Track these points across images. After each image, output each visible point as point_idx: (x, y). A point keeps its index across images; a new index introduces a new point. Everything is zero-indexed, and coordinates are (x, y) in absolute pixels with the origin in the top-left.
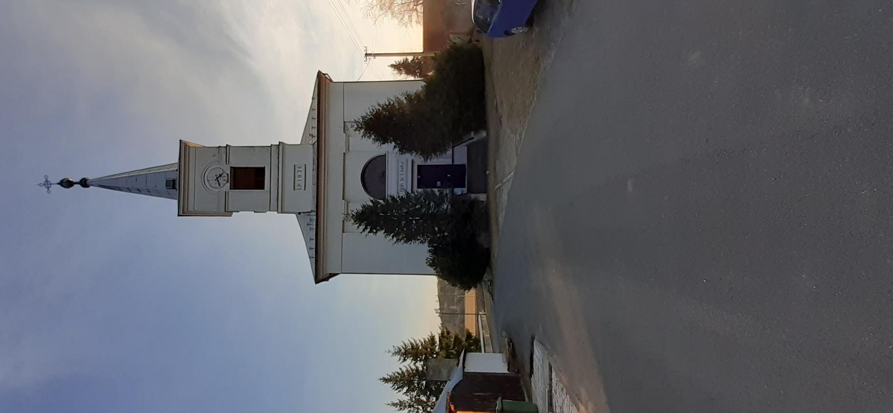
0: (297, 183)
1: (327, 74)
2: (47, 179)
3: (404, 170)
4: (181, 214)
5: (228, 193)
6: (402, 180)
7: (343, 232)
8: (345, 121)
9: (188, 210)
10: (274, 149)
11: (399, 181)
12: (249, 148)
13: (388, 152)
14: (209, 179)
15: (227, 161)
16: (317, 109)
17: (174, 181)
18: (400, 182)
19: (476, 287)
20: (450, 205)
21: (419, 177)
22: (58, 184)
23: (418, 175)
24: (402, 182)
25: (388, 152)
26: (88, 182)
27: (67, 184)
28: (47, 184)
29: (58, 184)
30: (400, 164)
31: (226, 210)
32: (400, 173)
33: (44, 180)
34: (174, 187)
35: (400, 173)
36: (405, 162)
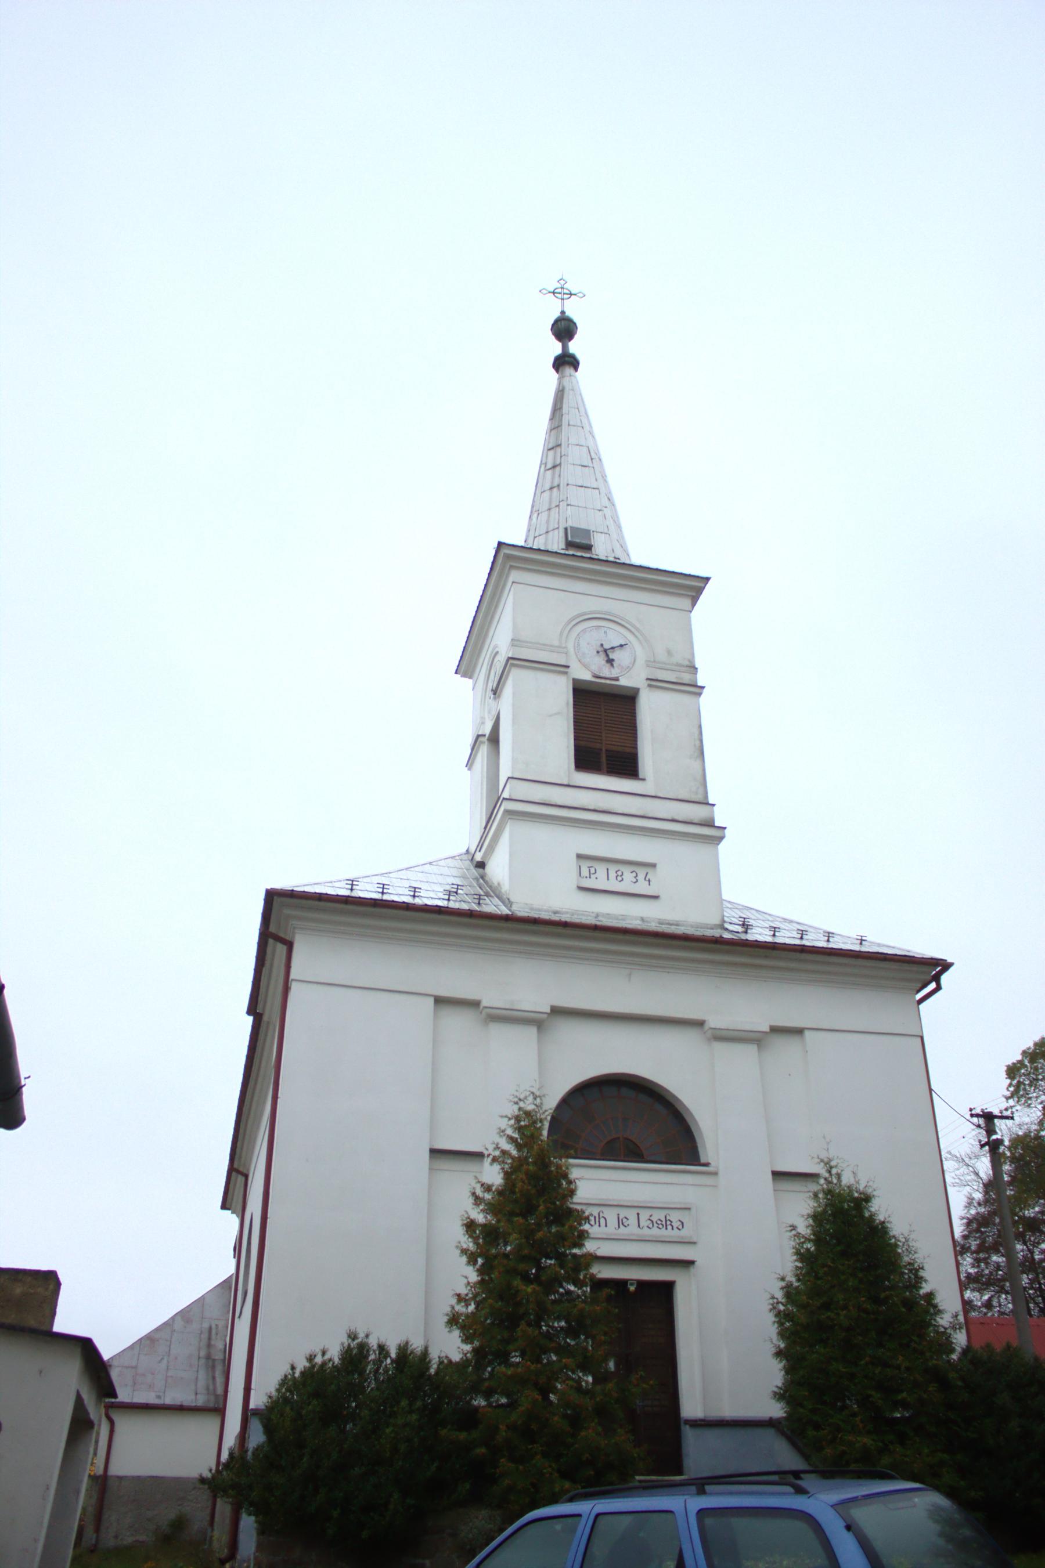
0: (601, 869)
1: (938, 988)
2: (575, 295)
3: (655, 1231)
4: (505, 551)
5: (566, 673)
6: (620, 1222)
7: (440, 1001)
8: (807, 1033)
9: (511, 567)
10: (697, 812)
11: (616, 1211)
12: (697, 732)
13: (715, 1174)
14: (603, 630)
15: (654, 683)
16: (831, 945)
17: (588, 548)
18: (611, 1215)
19: (419, 1356)
20: (248, 1523)
21: (632, 1288)
22: (563, 312)
23: (642, 1284)
24: (612, 1221)
25: (715, 1174)
26: (568, 370)
27: (564, 329)
28: (562, 293)
29: (563, 312)
30: (674, 1217)
31: (511, 661)
32: (644, 1215)
33: (571, 286)
34: (570, 544)
35: (644, 1215)
36: (685, 1233)
